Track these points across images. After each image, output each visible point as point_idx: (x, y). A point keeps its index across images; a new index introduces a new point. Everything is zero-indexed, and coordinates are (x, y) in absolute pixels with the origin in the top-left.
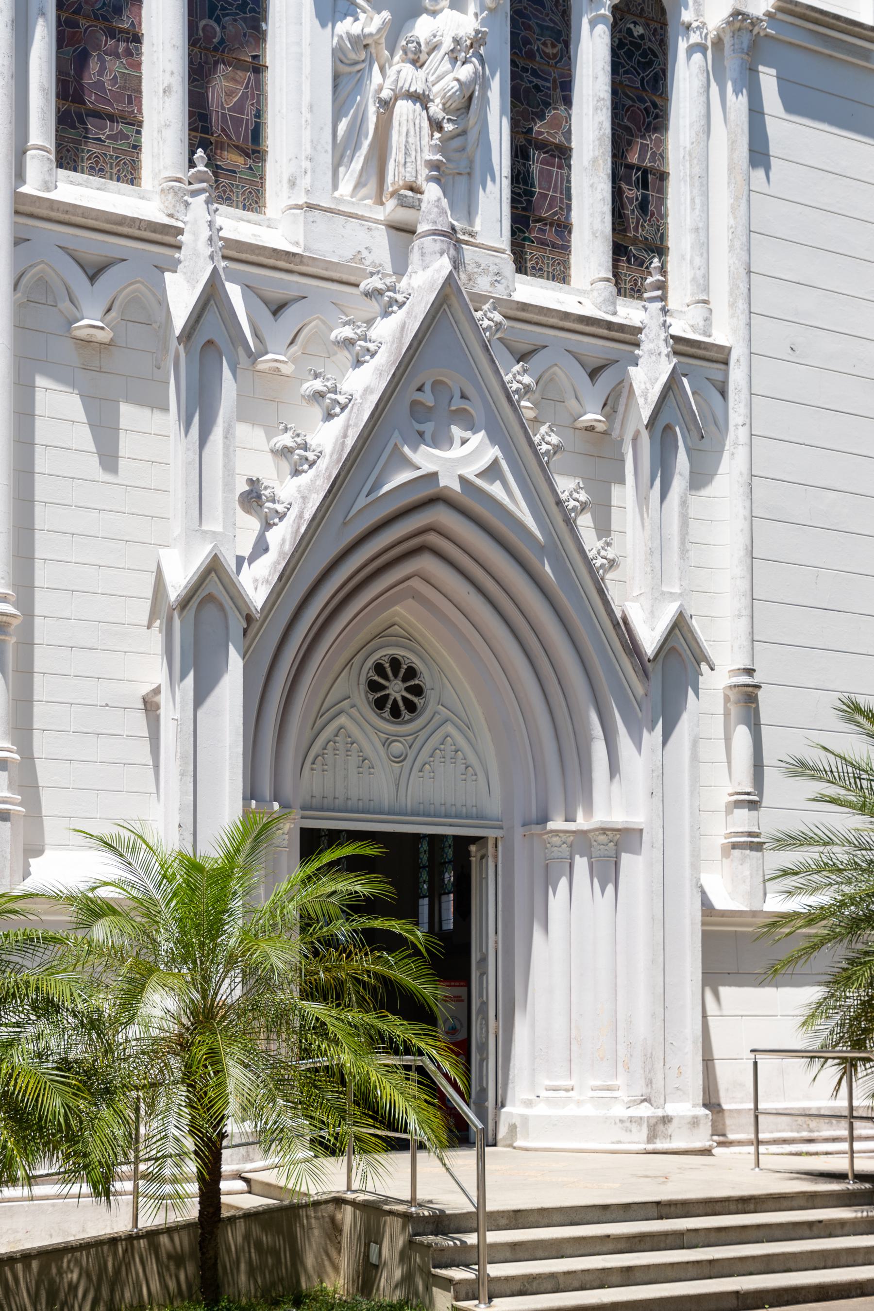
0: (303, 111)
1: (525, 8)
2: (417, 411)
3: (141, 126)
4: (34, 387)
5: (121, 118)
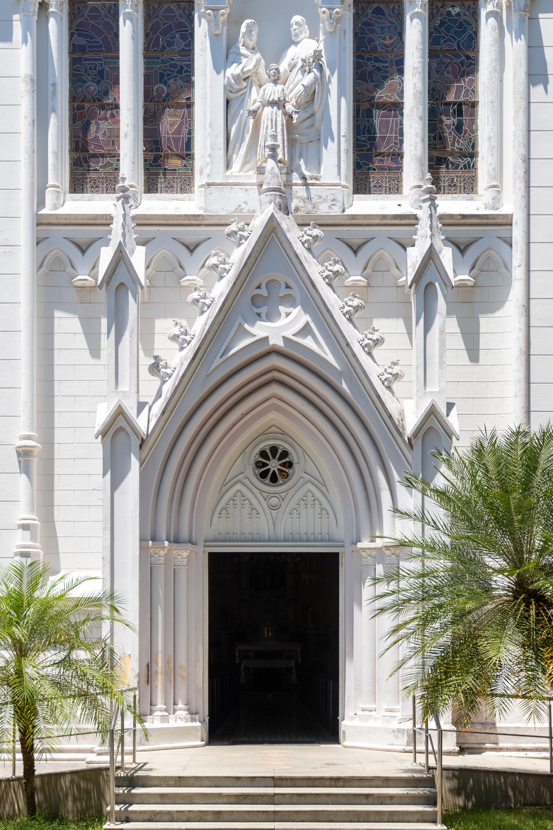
2: (255, 301)
3: (119, 157)
4: (53, 318)
5: (108, 154)
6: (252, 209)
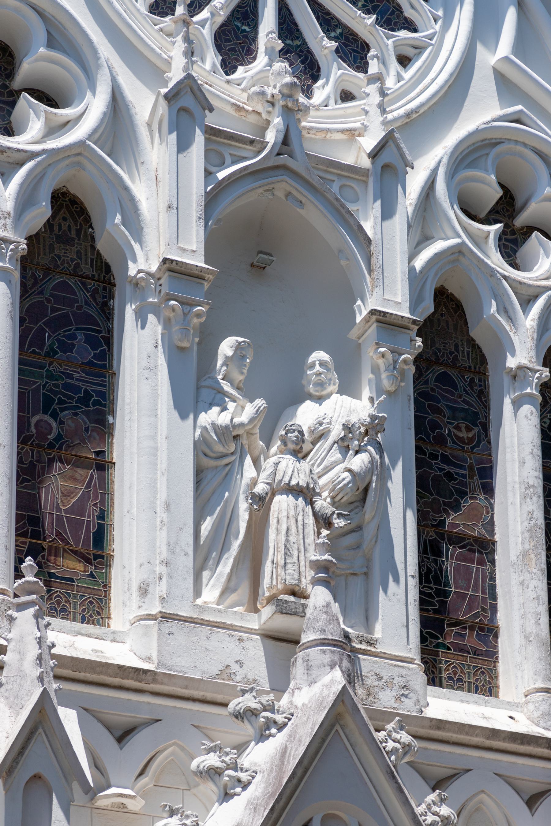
0: (158, 511)
1: (433, 390)
6: (251, 678)
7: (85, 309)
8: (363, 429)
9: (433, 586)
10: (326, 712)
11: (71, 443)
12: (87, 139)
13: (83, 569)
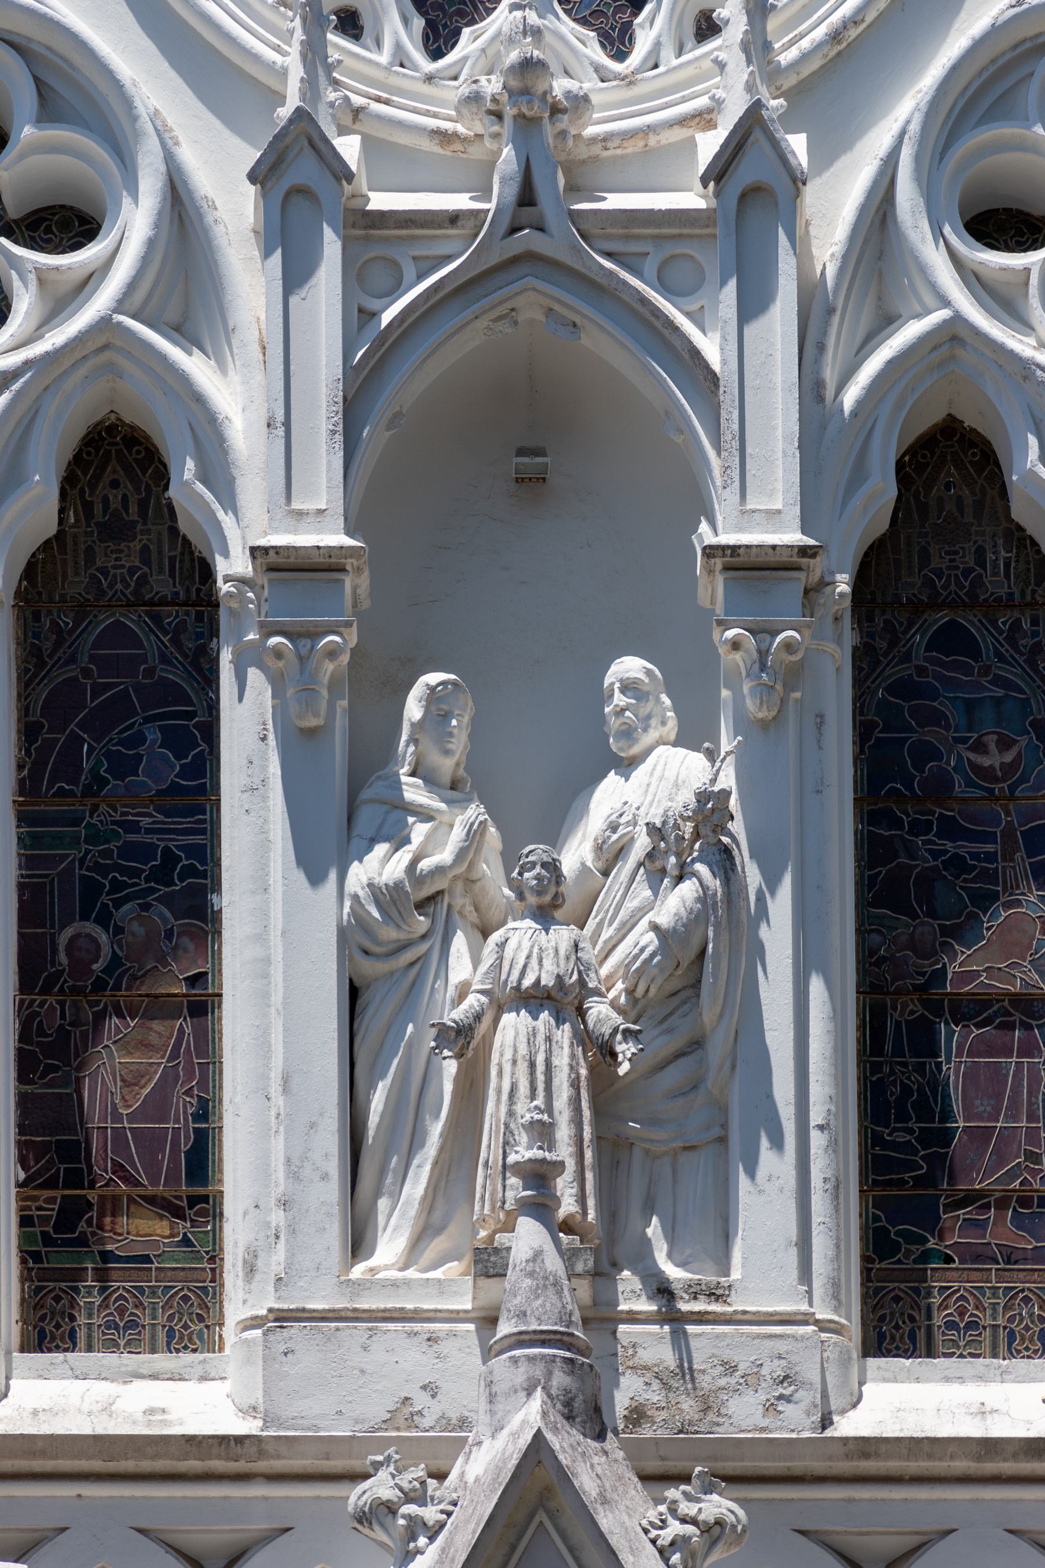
0: (273, 1095)
1: (921, 671)
6: (454, 1416)
7: (165, 673)
8: (688, 828)
9: (915, 1126)
10: (499, 1493)
11: (139, 970)
12: (117, 310)
13: (167, 1233)
